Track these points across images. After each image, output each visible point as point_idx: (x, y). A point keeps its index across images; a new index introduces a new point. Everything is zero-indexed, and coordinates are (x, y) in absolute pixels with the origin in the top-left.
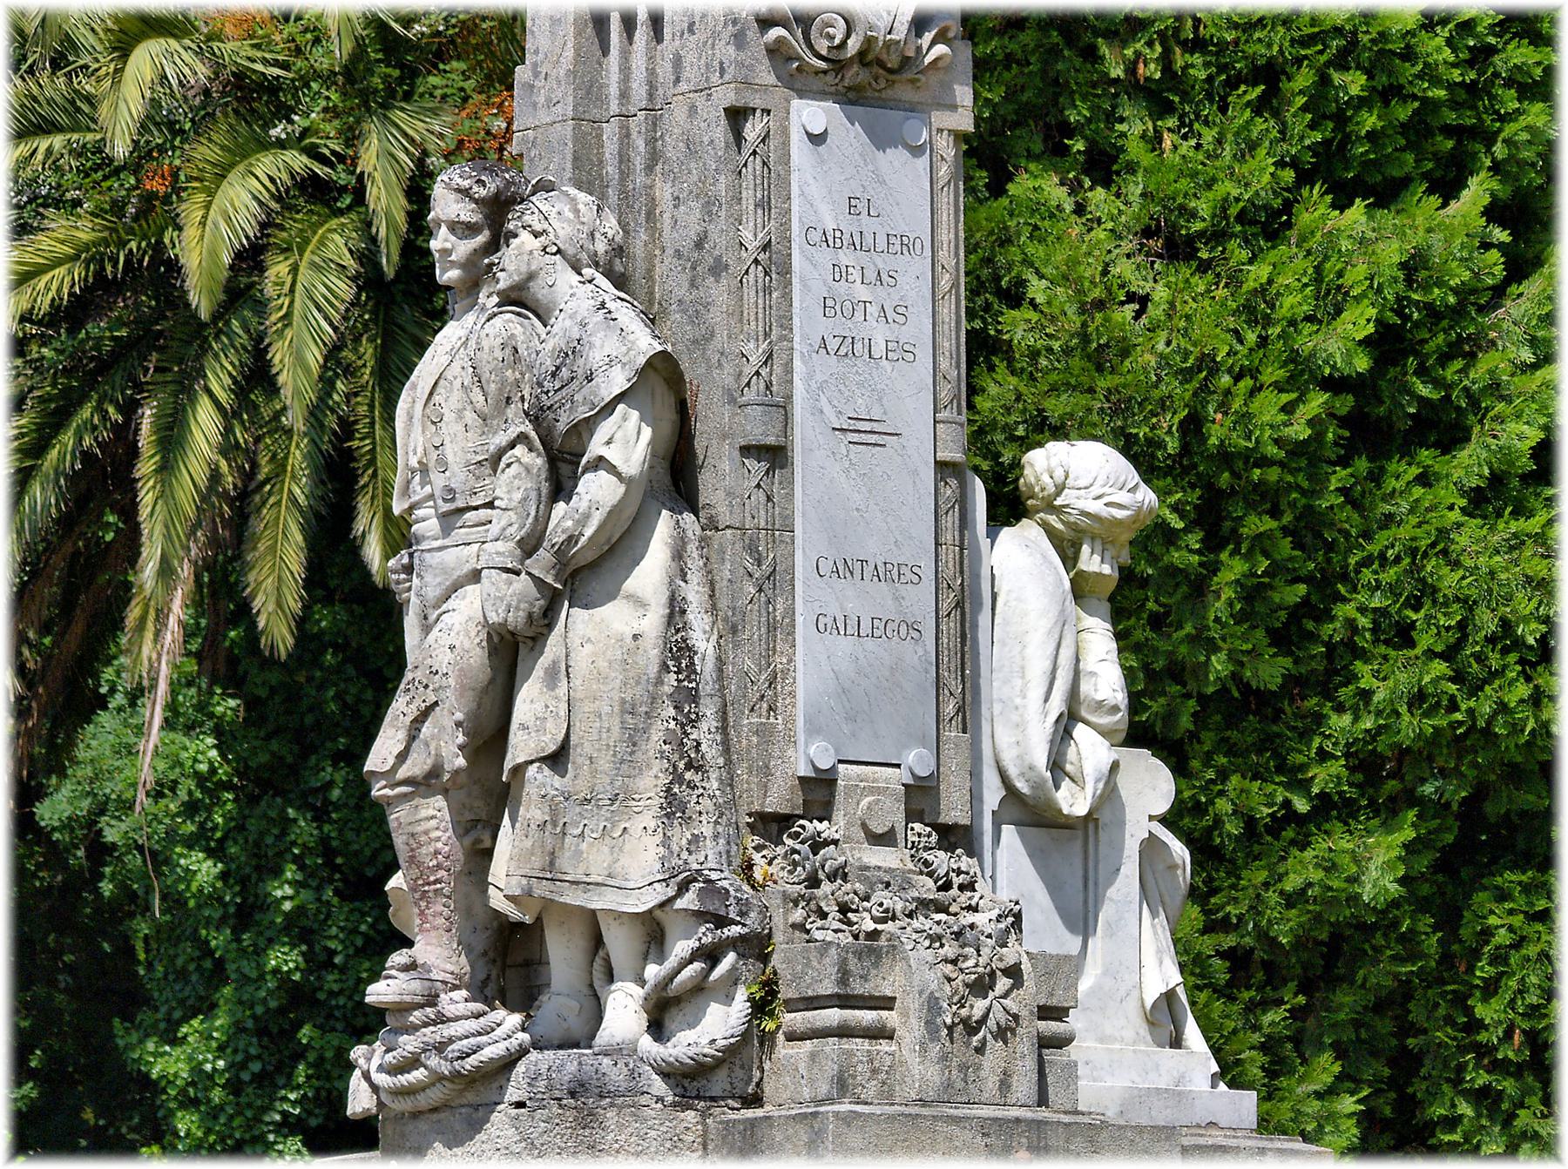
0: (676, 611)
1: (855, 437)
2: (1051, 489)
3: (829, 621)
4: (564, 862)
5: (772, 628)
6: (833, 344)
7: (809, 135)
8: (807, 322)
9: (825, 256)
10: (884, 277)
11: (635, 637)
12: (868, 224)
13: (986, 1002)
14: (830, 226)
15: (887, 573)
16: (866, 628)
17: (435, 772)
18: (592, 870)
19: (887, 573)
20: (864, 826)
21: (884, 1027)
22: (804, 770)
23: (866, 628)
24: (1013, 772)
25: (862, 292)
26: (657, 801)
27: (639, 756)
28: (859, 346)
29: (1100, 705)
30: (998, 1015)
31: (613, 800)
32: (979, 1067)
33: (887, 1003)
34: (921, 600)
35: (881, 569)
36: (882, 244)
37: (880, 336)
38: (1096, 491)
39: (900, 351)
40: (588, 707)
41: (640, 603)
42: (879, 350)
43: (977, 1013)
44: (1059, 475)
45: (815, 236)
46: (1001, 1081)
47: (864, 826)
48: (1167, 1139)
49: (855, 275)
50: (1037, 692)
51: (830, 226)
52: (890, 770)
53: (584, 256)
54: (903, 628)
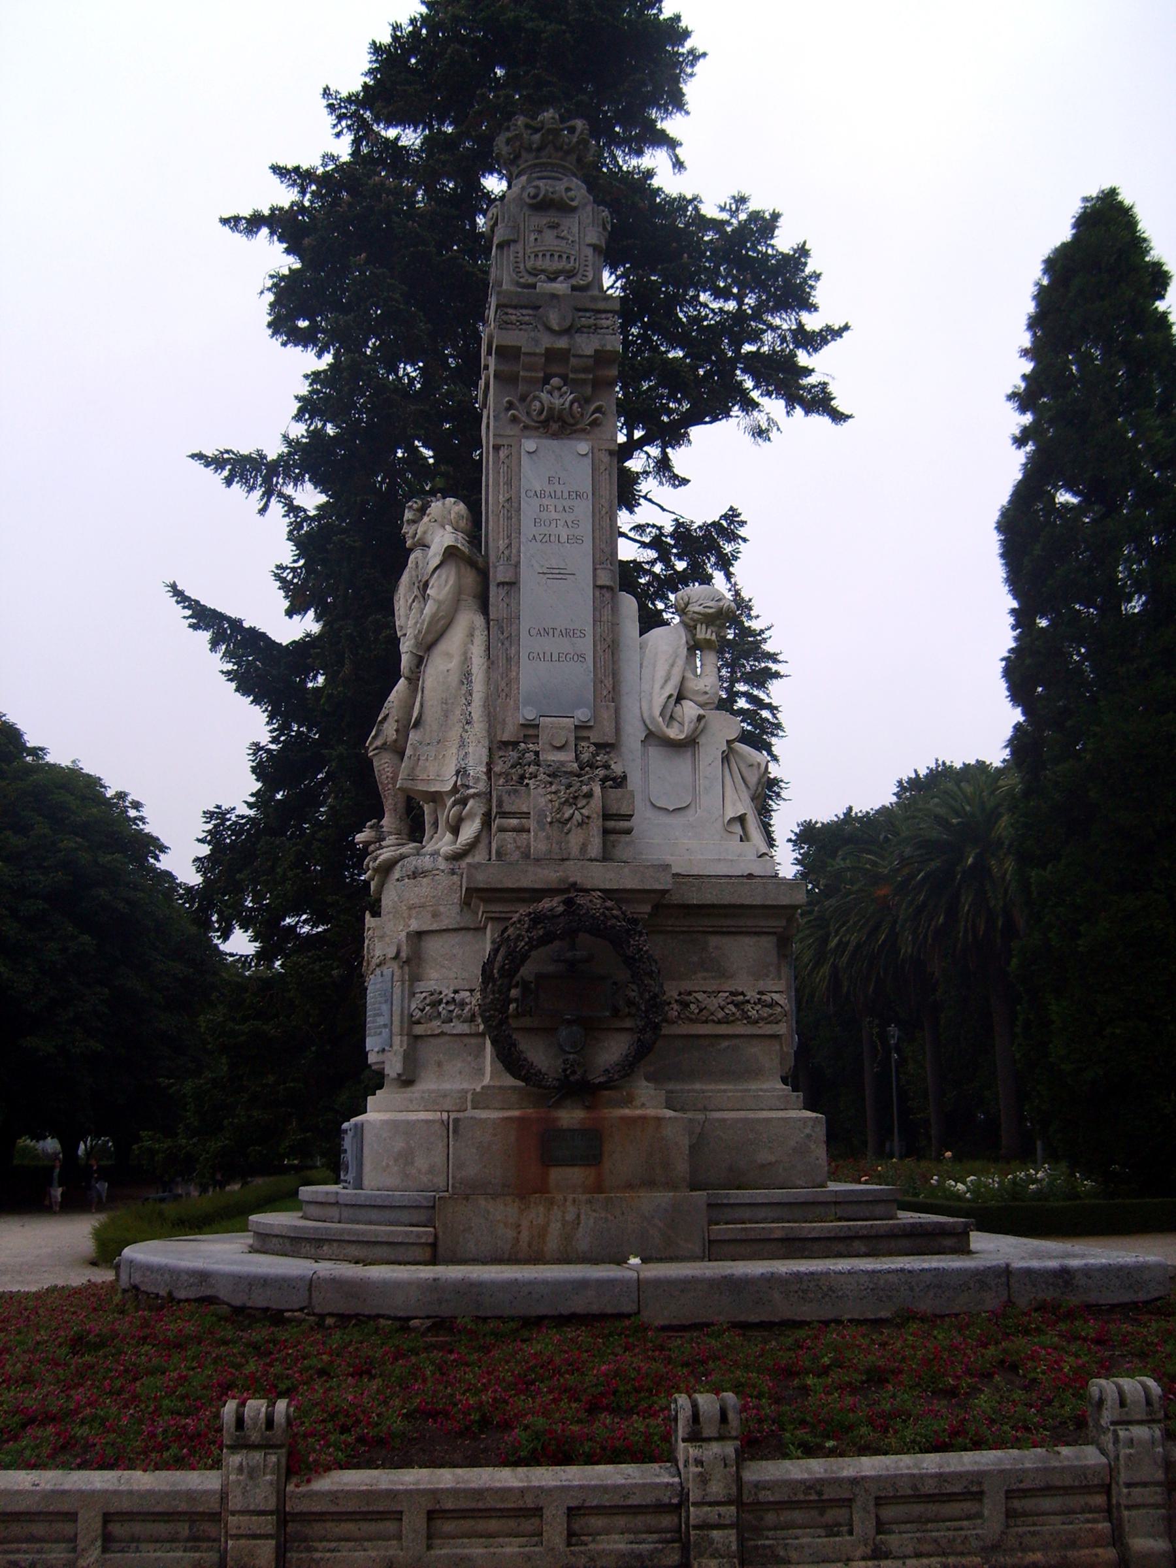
0: (466, 659)
1: (550, 576)
2: (683, 606)
3: (535, 655)
4: (417, 772)
5: (509, 659)
6: (539, 538)
7: (528, 452)
8: (528, 528)
9: (536, 502)
10: (567, 509)
11: (448, 671)
12: (558, 488)
13: (571, 811)
14: (538, 489)
15: (567, 633)
16: (555, 657)
17: (385, 744)
18: (431, 774)
19: (567, 633)
20: (551, 744)
21: (523, 826)
22: (522, 721)
23: (555, 657)
24: (648, 722)
25: (555, 515)
26: (457, 742)
27: (449, 722)
28: (552, 538)
29: (697, 692)
30: (577, 816)
31: (438, 743)
32: (568, 842)
33: (526, 815)
34: (586, 645)
35: (564, 632)
36: (566, 495)
37: (564, 534)
38: (699, 603)
39: (576, 540)
40: (430, 703)
41: (449, 655)
42: (564, 539)
43: (567, 815)
44: (686, 599)
45: (531, 494)
46: (581, 849)
47: (551, 744)
48: (663, 870)
49: (552, 508)
50: (657, 686)
51: (538, 489)
52: (568, 719)
53: (446, 521)
54: (576, 657)
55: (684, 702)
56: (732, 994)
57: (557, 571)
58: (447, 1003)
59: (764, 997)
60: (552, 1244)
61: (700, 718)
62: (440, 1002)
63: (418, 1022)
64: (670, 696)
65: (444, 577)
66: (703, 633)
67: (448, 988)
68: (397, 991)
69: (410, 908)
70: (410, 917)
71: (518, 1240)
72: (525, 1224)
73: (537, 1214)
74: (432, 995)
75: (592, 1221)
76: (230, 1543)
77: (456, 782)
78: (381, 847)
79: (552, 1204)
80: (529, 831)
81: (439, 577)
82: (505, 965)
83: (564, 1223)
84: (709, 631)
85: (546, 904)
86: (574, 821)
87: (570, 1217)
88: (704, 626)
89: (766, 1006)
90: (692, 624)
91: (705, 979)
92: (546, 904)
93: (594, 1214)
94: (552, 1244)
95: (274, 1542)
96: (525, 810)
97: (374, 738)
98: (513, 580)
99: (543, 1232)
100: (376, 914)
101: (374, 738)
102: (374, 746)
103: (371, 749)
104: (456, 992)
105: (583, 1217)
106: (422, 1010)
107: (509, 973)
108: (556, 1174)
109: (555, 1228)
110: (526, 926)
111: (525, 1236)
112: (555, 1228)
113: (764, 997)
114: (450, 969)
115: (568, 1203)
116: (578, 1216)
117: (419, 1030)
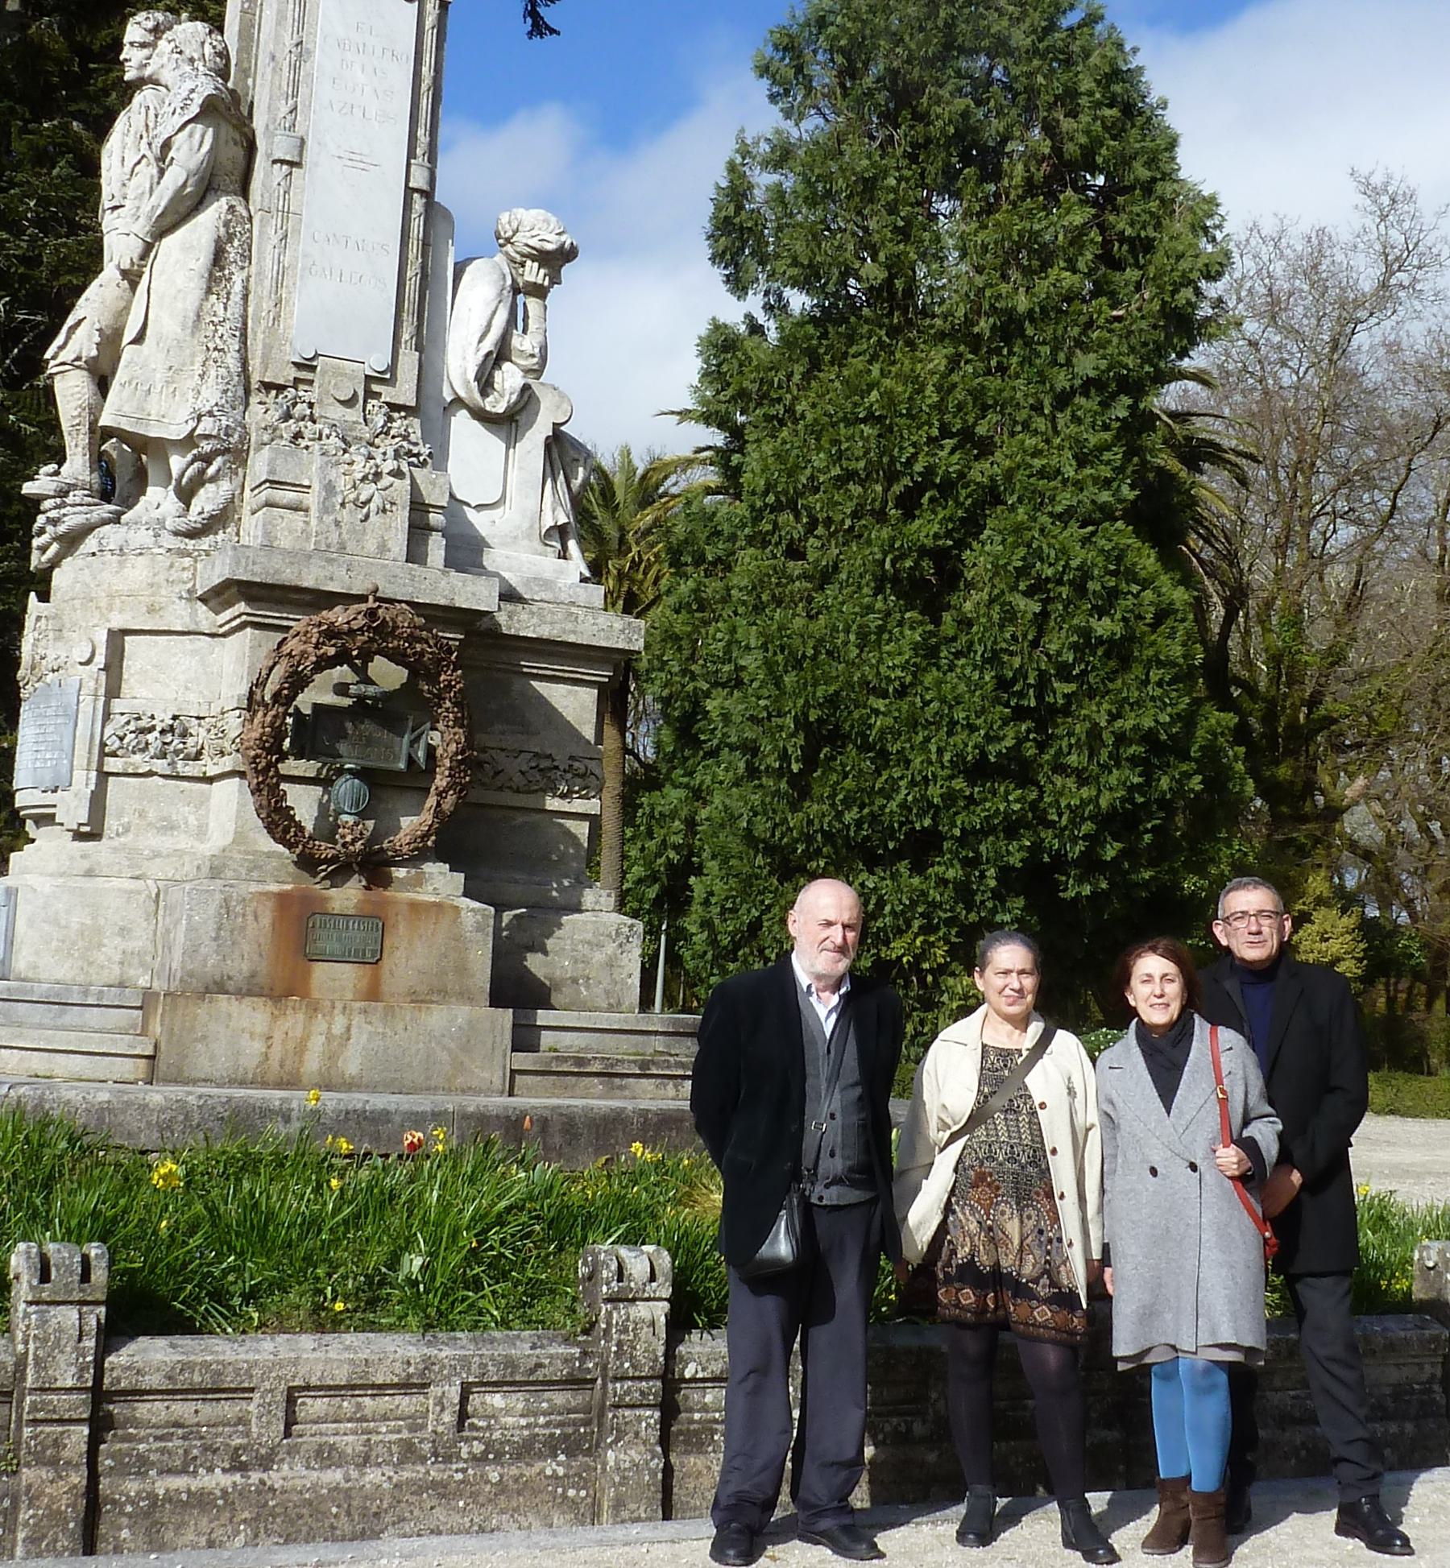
38: (534, 233)
55: (506, 366)
56: (536, 755)
57: (358, 158)
58: (163, 732)
59: (576, 765)
60: (312, 1063)
61: (526, 388)
62: (152, 729)
63: (114, 754)
64: (489, 353)
65: (197, 136)
66: (1061, 358)
67: (165, 711)
68: (86, 707)
69: (111, 596)
70: (110, 609)
71: (266, 1056)
72: (278, 1036)
73: (293, 1021)
74: (139, 719)
75: (365, 1037)
76: (27, 1431)
77: (194, 430)
78: (63, 505)
79: (315, 1010)
80: (306, 510)
81: (191, 135)
82: (281, 690)
83: (330, 1038)
84: (542, 271)
85: (339, 616)
86: (373, 506)
87: (338, 1028)
88: (536, 265)
89: (578, 775)
90: (518, 258)
91: (503, 733)
92: (339, 616)
93: (369, 1027)
94: (312, 1063)
95: (86, 1431)
96: (306, 483)
97: (62, 348)
98: (296, 159)
99: (301, 1048)
100: (44, 597)
101: (62, 348)
102: (59, 360)
103: (52, 363)
104: (175, 718)
105: (354, 1031)
106: (121, 739)
107: (283, 698)
108: (320, 971)
109: (317, 1043)
110: (314, 640)
111: (276, 1053)
112: (317, 1043)
113: (576, 765)
114: (168, 686)
115: (336, 1011)
116: (348, 1029)
117: (112, 765)
